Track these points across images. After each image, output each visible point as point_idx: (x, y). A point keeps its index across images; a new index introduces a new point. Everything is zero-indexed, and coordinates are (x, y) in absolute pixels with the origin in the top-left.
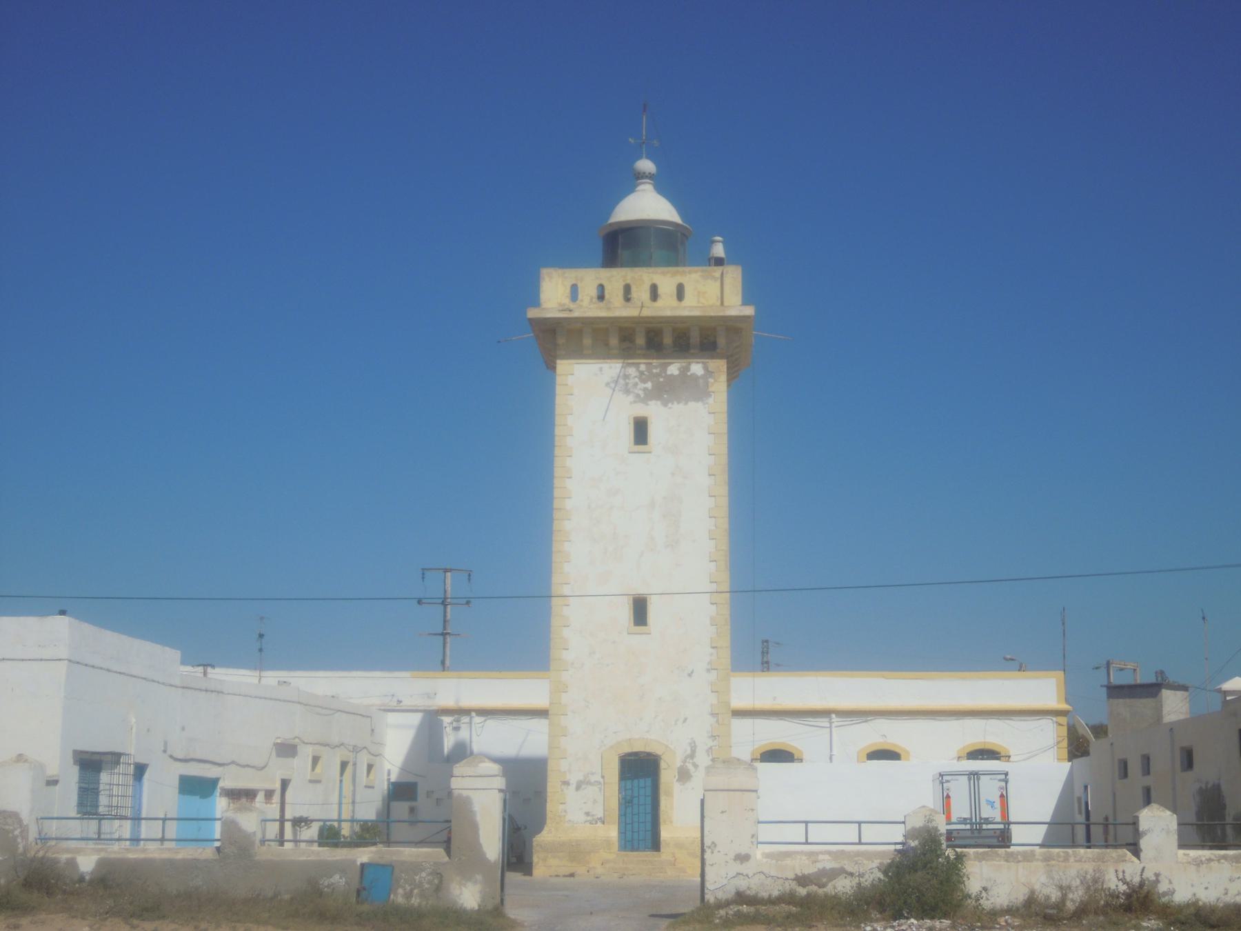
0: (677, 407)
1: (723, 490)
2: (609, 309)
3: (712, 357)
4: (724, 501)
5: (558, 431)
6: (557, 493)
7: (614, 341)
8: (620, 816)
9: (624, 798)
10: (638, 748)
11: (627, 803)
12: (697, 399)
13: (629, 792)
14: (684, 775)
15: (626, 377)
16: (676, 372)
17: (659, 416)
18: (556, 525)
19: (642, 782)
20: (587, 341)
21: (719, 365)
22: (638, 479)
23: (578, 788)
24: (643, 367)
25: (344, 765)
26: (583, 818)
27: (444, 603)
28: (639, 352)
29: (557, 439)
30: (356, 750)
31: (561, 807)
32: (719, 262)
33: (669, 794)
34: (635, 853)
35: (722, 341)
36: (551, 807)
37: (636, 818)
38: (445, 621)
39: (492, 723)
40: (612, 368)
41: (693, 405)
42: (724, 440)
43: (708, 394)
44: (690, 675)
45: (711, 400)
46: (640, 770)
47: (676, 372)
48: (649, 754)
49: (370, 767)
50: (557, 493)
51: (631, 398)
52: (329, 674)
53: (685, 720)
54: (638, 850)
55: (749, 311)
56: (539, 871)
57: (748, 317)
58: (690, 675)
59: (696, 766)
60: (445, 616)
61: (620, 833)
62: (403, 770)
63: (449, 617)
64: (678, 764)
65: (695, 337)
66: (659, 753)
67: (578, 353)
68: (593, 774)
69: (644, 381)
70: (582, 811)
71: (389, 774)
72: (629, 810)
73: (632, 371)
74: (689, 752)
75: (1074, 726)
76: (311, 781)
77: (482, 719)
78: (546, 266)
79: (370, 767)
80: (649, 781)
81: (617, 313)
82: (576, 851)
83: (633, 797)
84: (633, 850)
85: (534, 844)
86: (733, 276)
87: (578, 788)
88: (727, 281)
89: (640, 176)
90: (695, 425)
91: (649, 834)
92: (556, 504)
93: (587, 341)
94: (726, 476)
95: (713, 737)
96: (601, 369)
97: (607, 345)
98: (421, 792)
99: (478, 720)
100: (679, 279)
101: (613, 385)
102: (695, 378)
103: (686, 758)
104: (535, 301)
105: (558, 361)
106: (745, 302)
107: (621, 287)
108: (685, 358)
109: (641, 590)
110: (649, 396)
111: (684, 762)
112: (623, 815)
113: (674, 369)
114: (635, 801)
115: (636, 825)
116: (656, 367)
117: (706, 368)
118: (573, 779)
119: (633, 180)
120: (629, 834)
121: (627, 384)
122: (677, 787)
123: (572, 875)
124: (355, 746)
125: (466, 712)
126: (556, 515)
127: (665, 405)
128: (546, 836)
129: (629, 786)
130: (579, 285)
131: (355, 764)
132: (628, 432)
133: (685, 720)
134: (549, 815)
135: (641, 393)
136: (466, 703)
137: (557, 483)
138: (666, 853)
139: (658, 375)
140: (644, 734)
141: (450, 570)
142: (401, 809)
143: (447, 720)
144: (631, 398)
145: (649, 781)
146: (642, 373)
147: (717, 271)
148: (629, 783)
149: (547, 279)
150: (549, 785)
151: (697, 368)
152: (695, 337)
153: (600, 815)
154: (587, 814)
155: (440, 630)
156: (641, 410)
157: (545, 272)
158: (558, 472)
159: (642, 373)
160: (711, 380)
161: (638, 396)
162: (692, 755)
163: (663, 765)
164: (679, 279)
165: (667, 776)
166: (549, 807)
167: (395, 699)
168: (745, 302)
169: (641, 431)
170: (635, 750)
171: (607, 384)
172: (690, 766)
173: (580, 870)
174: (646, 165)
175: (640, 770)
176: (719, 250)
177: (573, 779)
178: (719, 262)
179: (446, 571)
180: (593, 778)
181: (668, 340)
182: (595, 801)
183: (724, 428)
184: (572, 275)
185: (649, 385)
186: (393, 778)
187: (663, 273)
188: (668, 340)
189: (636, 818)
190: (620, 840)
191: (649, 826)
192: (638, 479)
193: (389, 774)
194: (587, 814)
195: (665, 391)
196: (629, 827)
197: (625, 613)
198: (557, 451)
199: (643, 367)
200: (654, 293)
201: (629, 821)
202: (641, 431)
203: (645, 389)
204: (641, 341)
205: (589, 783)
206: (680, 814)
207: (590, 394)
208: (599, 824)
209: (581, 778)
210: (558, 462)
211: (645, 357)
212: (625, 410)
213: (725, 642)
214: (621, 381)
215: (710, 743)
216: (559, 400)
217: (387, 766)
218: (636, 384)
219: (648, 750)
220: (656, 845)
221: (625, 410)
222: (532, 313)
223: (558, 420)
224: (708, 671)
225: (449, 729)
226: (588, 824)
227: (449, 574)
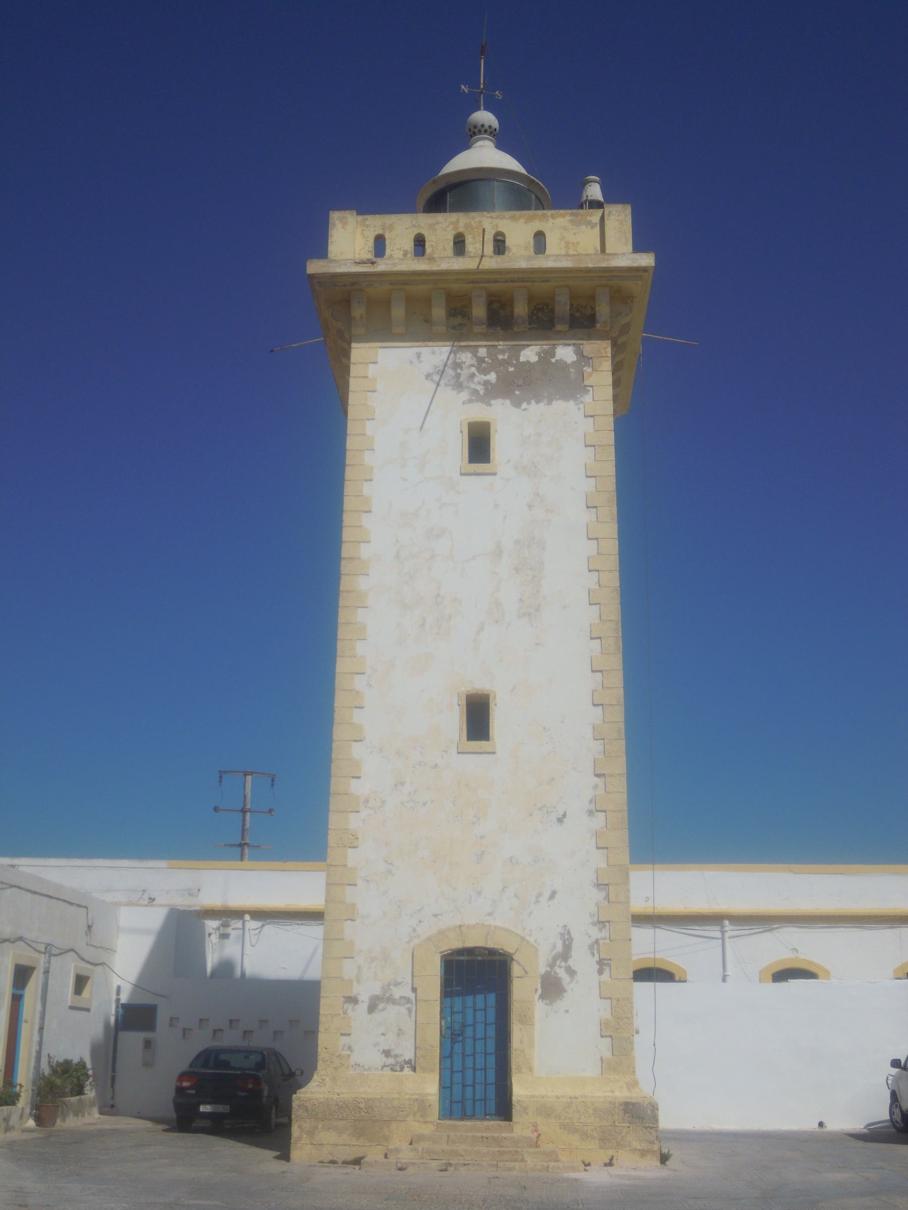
0: (535, 409)
1: (611, 530)
2: (432, 259)
3: (590, 338)
4: (612, 546)
5: (352, 443)
6: (347, 534)
7: (439, 312)
8: (442, 1058)
9: (450, 1028)
10: (471, 942)
11: (452, 1036)
12: (566, 397)
13: (458, 1018)
14: (552, 988)
15: (457, 365)
16: (534, 359)
17: (508, 421)
18: (345, 583)
19: (480, 998)
20: (398, 312)
21: (601, 350)
22: (476, 522)
23: (372, 1008)
24: (482, 352)
25: (22, 975)
26: (379, 1060)
27: (244, 811)
28: (477, 329)
29: (349, 455)
30: (49, 950)
31: (345, 1040)
32: (595, 205)
33: (527, 1020)
34: (468, 1123)
35: (603, 310)
36: (327, 1040)
37: (469, 1062)
38: (243, 831)
39: (271, 930)
40: (436, 354)
41: (559, 405)
42: (610, 455)
43: (584, 389)
44: (560, 821)
45: (588, 398)
46: (477, 978)
47: (534, 359)
48: (492, 952)
49: (81, 982)
50: (347, 534)
51: (464, 395)
52: (62, 862)
53: (553, 895)
54: (472, 1117)
55: (647, 260)
56: (303, 1150)
57: (645, 269)
58: (560, 821)
59: (571, 972)
60: (244, 825)
61: (442, 1087)
62: (138, 987)
63: (248, 825)
64: (543, 969)
65: (563, 307)
66: (510, 949)
67: (384, 331)
68: (397, 984)
69: (485, 372)
70: (375, 1052)
71: (118, 993)
72: (458, 1047)
73: (466, 357)
74: (560, 948)
75: (773, 975)
76: (71, 1008)
77: (258, 924)
78: (343, 206)
79: (81, 982)
80: (492, 998)
81: (444, 266)
82: (366, 1119)
83: (464, 1025)
84: (464, 1116)
85: (295, 1104)
86: (620, 219)
87: (372, 1008)
88: (610, 224)
89: (477, 131)
90: (563, 440)
91: (492, 1090)
92: (346, 551)
93: (398, 312)
94: (615, 510)
95: (601, 924)
96: (419, 355)
97: (428, 321)
98: (162, 1018)
99: (252, 924)
100: (537, 226)
101: (437, 378)
102: (562, 366)
103: (555, 959)
104: (321, 251)
105: (353, 345)
106: (638, 247)
107: (451, 237)
108: (548, 338)
109: (480, 685)
110: (491, 393)
111: (552, 965)
112: (446, 1056)
113: (530, 354)
114: (469, 1031)
115: (469, 1073)
116: (503, 352)
117: (579, 353)
118: (365, 992)
119: (466, 137)
120: (457, 1089)
121: (458, 376)
122: (540, 1008)
123: (357, 1162)
124: (48, 945)
125: (238, 914)
126: (345, 567)
127: (517, 404)
128: (312, 1093)
129: (458, 1006)
130: (387, 236)
131: (46, 972)
132: (459, 446)
133: (553, 895)
134: (322, 1054)
135: (481, 389)
136: (236, 901)
137: (347, 519)
138: (521, 1125)
139: (507, 363)
140: (483, 919)
141: (251, 773)
142: (133, 1040)
143: (211, 924)
144: (464, 395)
145: (492, 998)
146: (481, 360)
147: (595, 216)
148: (458, 1001)
149: (339, 225)
150: (323, 1002)
151: (565, 353)
152: (563, 307)
153: (409, 1055)
154: (387, 1053)
155: (238, 840)
156: (479, 412)
157: (335, 216)
158: (349, 503)
159: (481, 360)
160: (588, 370)
161: (475, 392)
162: (565, 954)
163: (516, 970)
164: (537, 226)
165: (523, 989)
166: (323, 1039)
167: (146, 896)
168: (638, 247)
169: (479, 445)
170: (470, 944)
171: (428, 376)
172: (561, 973)
173: (374, 1154)
174: (484, 117)
175: (477, 978)
176: (594, 191)
177: (365, 992)
178: (595, 205)
179: (246, 774)
180: (397, 993)
181: (521, 309)
182: (400, 1033)
183: (609, 438)
184: (376, 223)
185: (492, 377)
186: (124, 999)
187: (514, 218)
188: (521, 309)
189: (469, 1062)
190: (442, 1098)
191: (491, 1077)
192: (476, 522)
193: (118, 993)
194: (387, 1053)
195: (516, 385)
196: (458, 1077)
197: (454, 721)
198: (349, 473)
199: (482, 352)
200: (500, 245)
201: (457, 1066)
202: (479, 445)
203: (486, 383)
204: (479, 311)
205: (391, 1000)
206: (554, 1052)
207: (402, 402)
208: (407, 1071)
209: (378, 991)
210: (349, 489)
211: (484, 336)
212: (455, 412)
213: (619, 766)
214: (450, 372)
215: (595, 933)
216: (354, 399)
217: (116, 982)
218: (472, 376)
219: (490, 945)
220: (504, 1109)
221: (455, 412)
222: (314, 267)
223: (352, 427)
224: (591, 813)
225: (214, 938)
226: (387, 1072)
227: (249, 778)
